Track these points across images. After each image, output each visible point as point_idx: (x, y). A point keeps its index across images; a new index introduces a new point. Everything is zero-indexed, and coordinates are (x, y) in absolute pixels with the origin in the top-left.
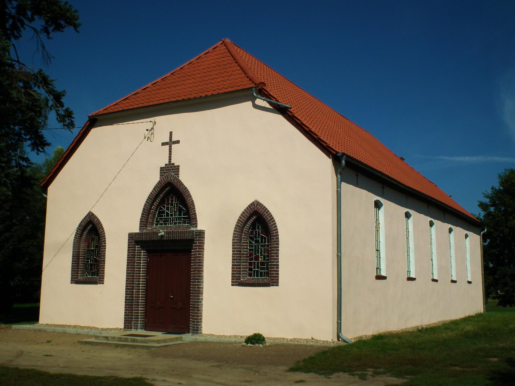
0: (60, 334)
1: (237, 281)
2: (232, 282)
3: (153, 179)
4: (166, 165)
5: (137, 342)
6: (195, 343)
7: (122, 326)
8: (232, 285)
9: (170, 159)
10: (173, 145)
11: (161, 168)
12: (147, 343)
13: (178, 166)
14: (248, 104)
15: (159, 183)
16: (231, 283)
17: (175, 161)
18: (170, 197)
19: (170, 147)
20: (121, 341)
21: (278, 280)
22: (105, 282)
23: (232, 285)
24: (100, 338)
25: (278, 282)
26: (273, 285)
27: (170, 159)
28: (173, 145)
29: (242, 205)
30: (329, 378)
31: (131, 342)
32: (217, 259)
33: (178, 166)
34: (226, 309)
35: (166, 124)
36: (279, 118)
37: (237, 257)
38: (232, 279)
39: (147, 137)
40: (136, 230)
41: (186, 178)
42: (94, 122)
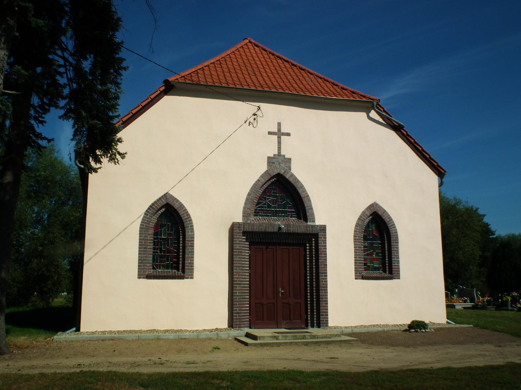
0: (114, 341)
1: (360, 275)
2: (355, 276)
3: (258, 169)
4: (274, 155)
5: (317, 338)
6: (67, 364)
7: (224, 324)
8: (356, 279)
9: (279, 148)
10: (282, 131)
11: (269, 158)
12: (330, 338)
13: (290, 159)
14: (364, 115)
15: (266, 172)
16: (354, 277)
17: (286, 152)
18: (280, 192)
19: (279, 130)
20: (297, 339)
21: (399, 274)
22: (194, 276)
23: (356, 279)
24: (266, 339)
25: (399, 276)
26: (395, 279)
27: (279, 148)
28: (282, 131)
29: (361, 206)
30: (394, 349)
31: (311, 338)
32: (340, 255)
33: (290, 159)
34: (353, 302)
35: (273, 113)
36: (391, 136)
37: (359, 252)
38: (355, 273)
39: (248, 122)
40: (239, 219)
41: (301, 173)
42: (169, 89)
